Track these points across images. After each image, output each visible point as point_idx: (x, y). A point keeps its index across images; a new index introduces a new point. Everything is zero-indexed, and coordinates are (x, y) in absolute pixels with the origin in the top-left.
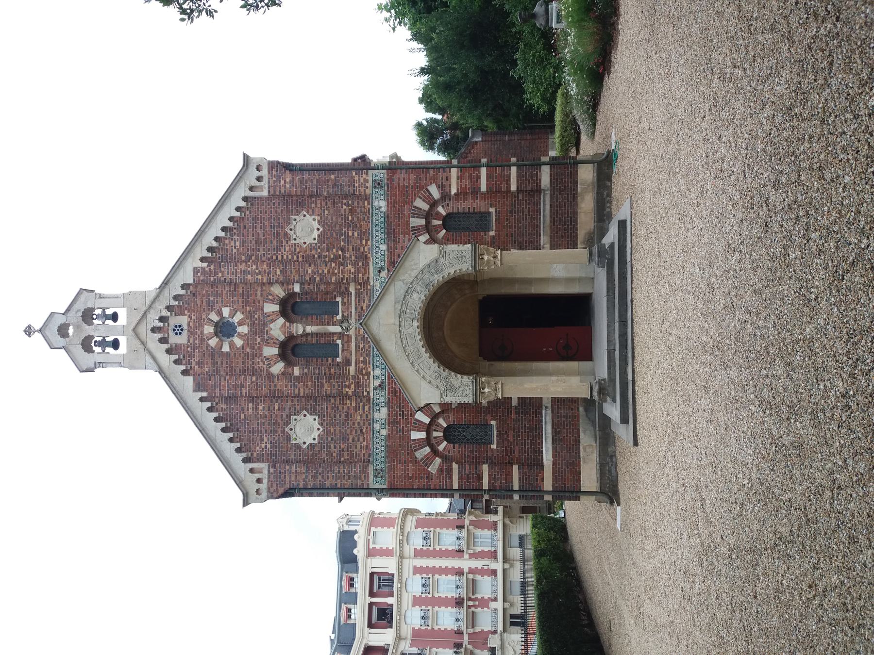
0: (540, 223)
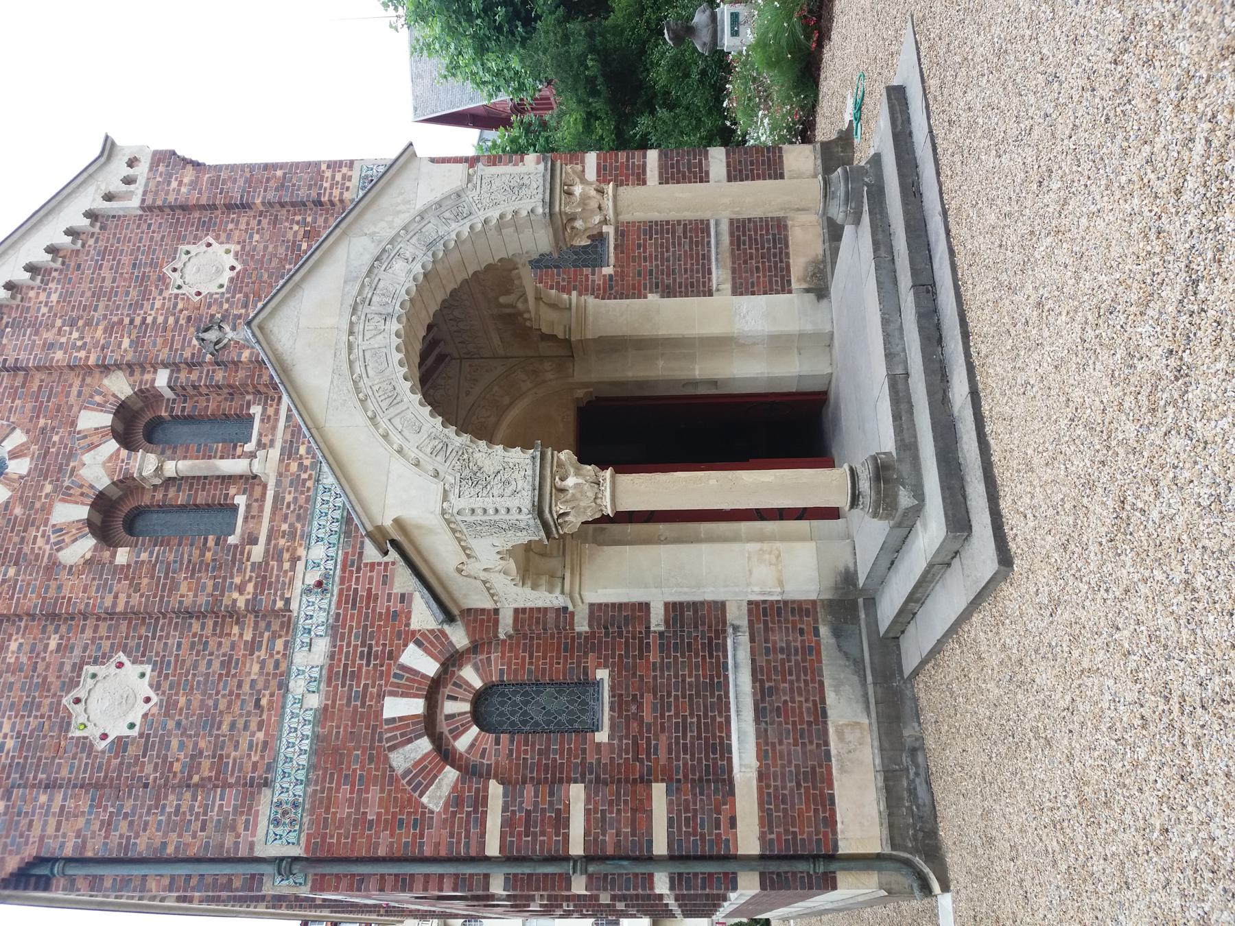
0: (709, 251)
